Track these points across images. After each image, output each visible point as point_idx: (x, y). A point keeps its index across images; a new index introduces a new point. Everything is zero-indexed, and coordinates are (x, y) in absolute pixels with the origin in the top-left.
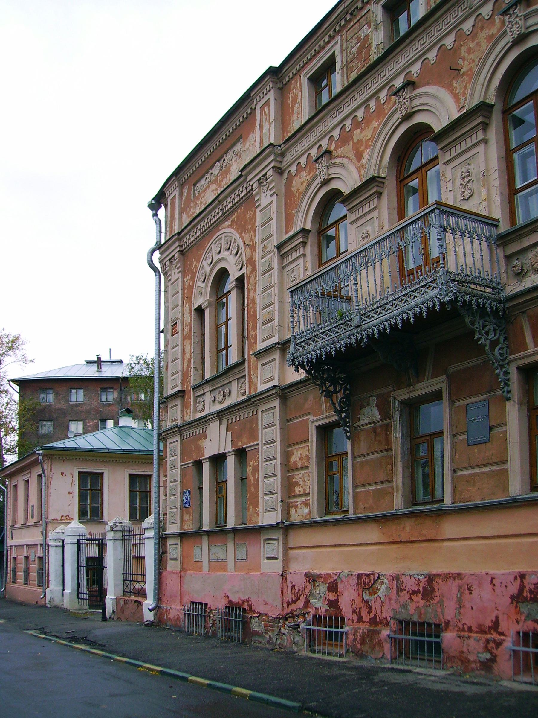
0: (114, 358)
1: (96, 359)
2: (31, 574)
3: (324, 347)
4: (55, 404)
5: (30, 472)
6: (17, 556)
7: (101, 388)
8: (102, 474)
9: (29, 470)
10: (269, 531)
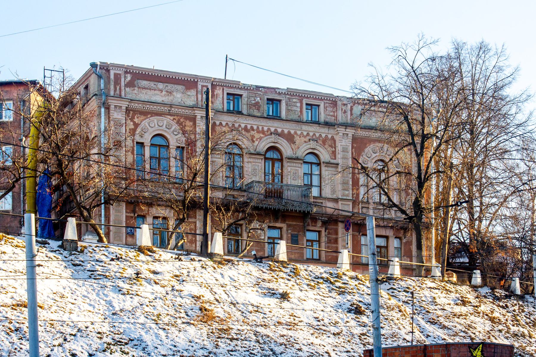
3: (269, 205)
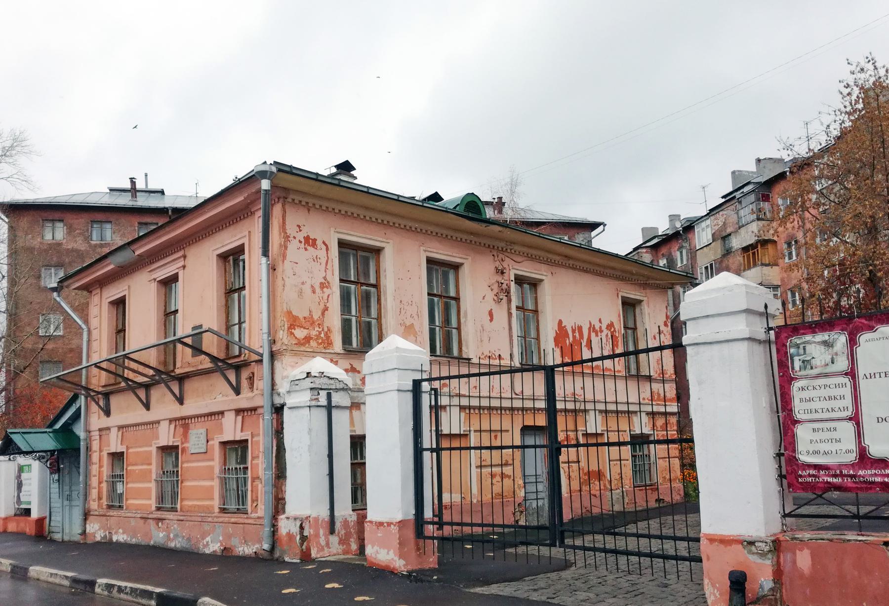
0: (151, 187)
1: (128, 185)
2: (187, 484)
4: (67, 242)
5: (185, 257)
6: (128, 448)
7: (139, 223)
8: (377, 251)
9: (181, 254)
10: (383, 564)
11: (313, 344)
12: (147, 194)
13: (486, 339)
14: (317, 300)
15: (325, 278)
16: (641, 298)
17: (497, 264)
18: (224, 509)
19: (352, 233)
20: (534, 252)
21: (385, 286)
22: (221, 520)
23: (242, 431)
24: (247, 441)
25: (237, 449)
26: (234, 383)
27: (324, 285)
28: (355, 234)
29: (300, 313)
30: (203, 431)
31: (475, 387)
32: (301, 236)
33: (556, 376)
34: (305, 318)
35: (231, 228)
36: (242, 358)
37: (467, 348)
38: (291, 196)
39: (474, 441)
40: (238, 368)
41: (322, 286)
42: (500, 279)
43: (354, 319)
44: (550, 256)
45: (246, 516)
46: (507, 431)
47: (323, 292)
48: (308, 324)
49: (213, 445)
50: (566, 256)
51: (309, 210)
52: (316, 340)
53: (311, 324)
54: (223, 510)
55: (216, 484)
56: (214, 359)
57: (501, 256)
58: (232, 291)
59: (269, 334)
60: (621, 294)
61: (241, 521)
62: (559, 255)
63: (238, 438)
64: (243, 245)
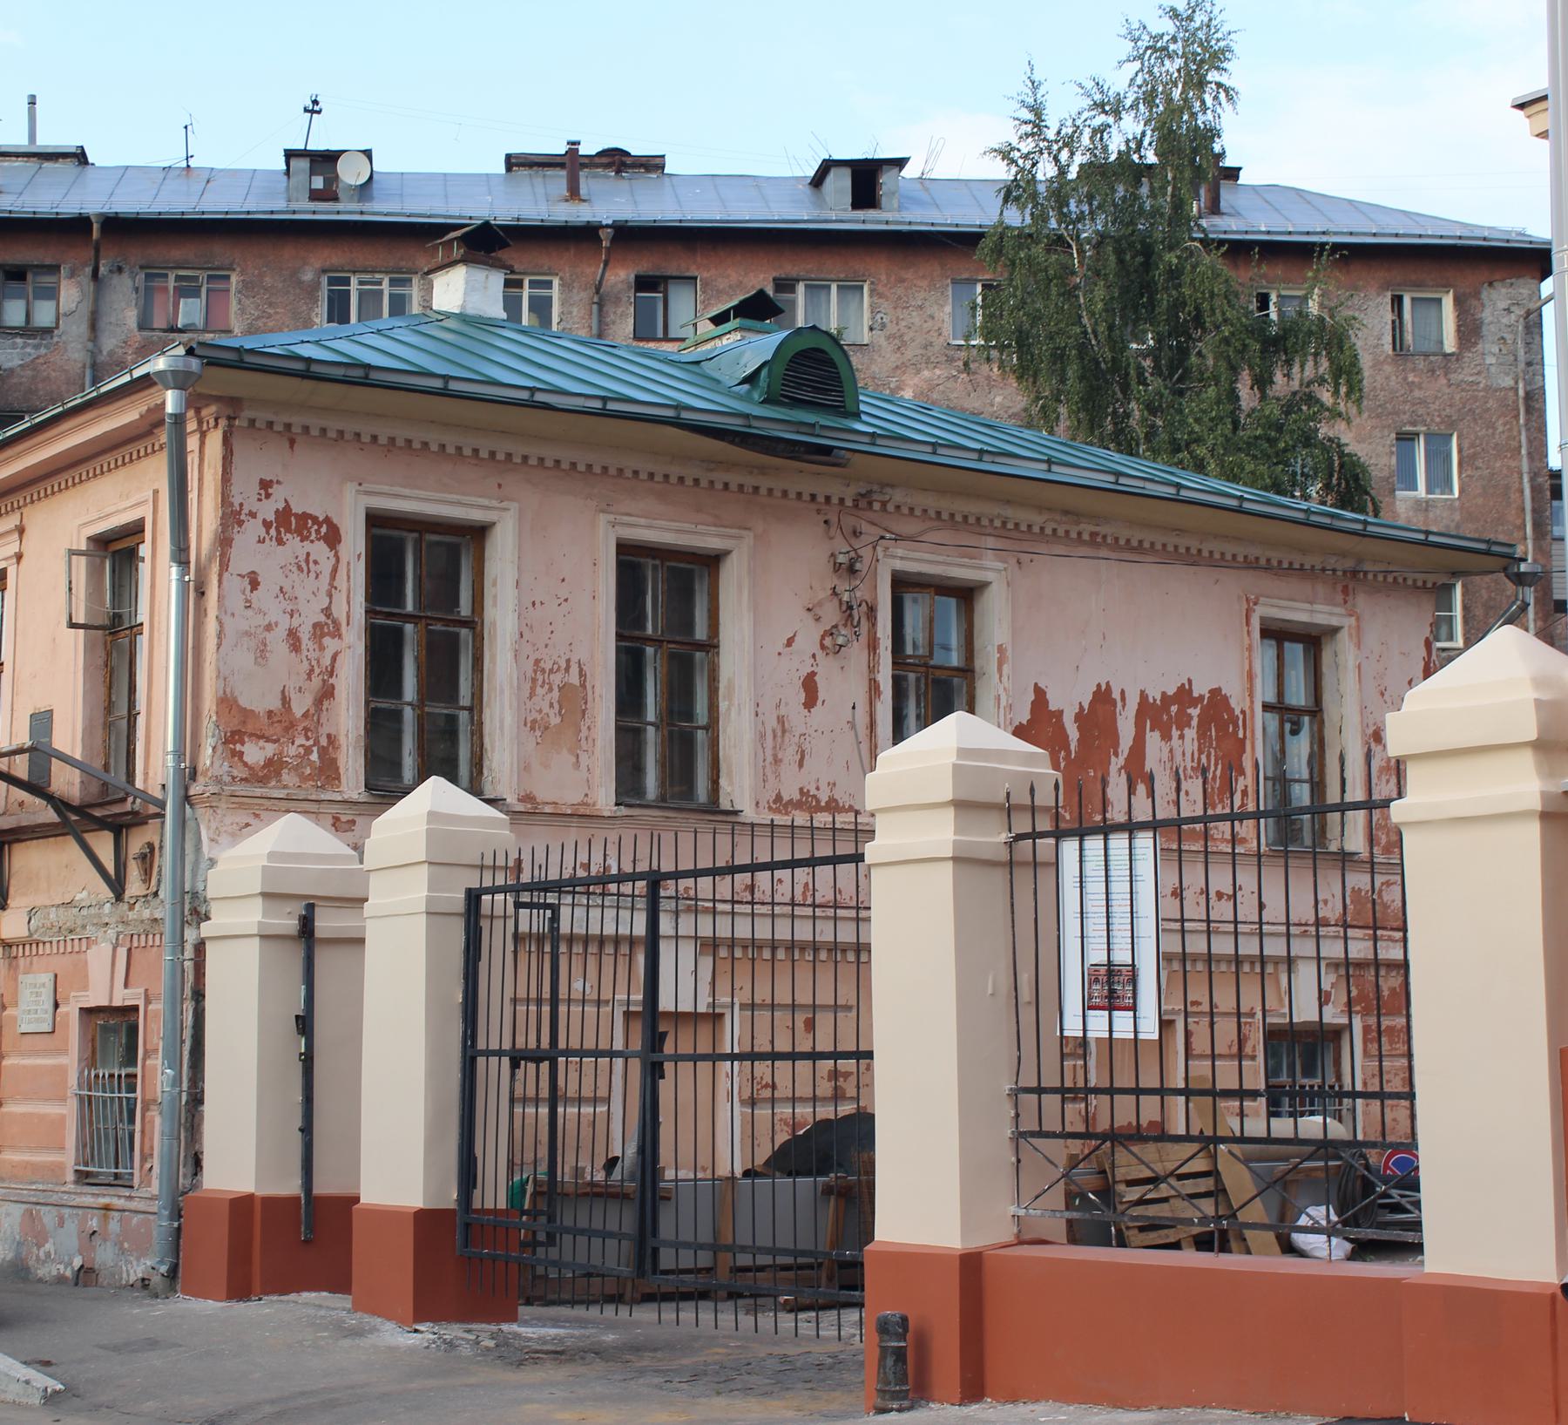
0: (48, 139)
5: (21, 530)
9: (12, 521)
11: (288, 778)
12: (33, 164)
13: (790, 755)
14: (305, 666)
15: (327, 611)
16: (1334, 622)
17: (841, 545)
18: (88, 1174)
19: (407, 492)
20: (961, 506)
21: (494, 624)
22: (79, 1200)
23: (126, 986)
24: (135, 1008)
25: (113, 1028)
26: (110, 867)
27: (327, 628)
28: (417, 492)
29: (259, 698)
30: (47, 979)
31: (780, 881)
32: (268, 510)
33: (662, 915)
34: (270, 713)
35: (122, 473)
36: (128, 807)
37: (731, 784)
38: (247, 414)
39: (733, 1036)
40: (120, 827)
41: (319, 631)
42: (843, 586)
43: (408, 714)
44: (1009, 512)
45: (127, 1192)
46: (848, 1008)
47: (322, 648)
48: (278, 728)
49: (67, 1014)
50: (1066, 512)
51: (292, 442)
52: (296, 768)
53: (287, 730)
54: (83, 1177)
55: (69, 1111)
56: (60, 804)
57: (849, 521)
58: (113, 637)
59: (179, 754)
60: (1260, 611)
61: (120, 1203)
62: (1040, 508)
63: (117, 1003)
64: (142, 520)
